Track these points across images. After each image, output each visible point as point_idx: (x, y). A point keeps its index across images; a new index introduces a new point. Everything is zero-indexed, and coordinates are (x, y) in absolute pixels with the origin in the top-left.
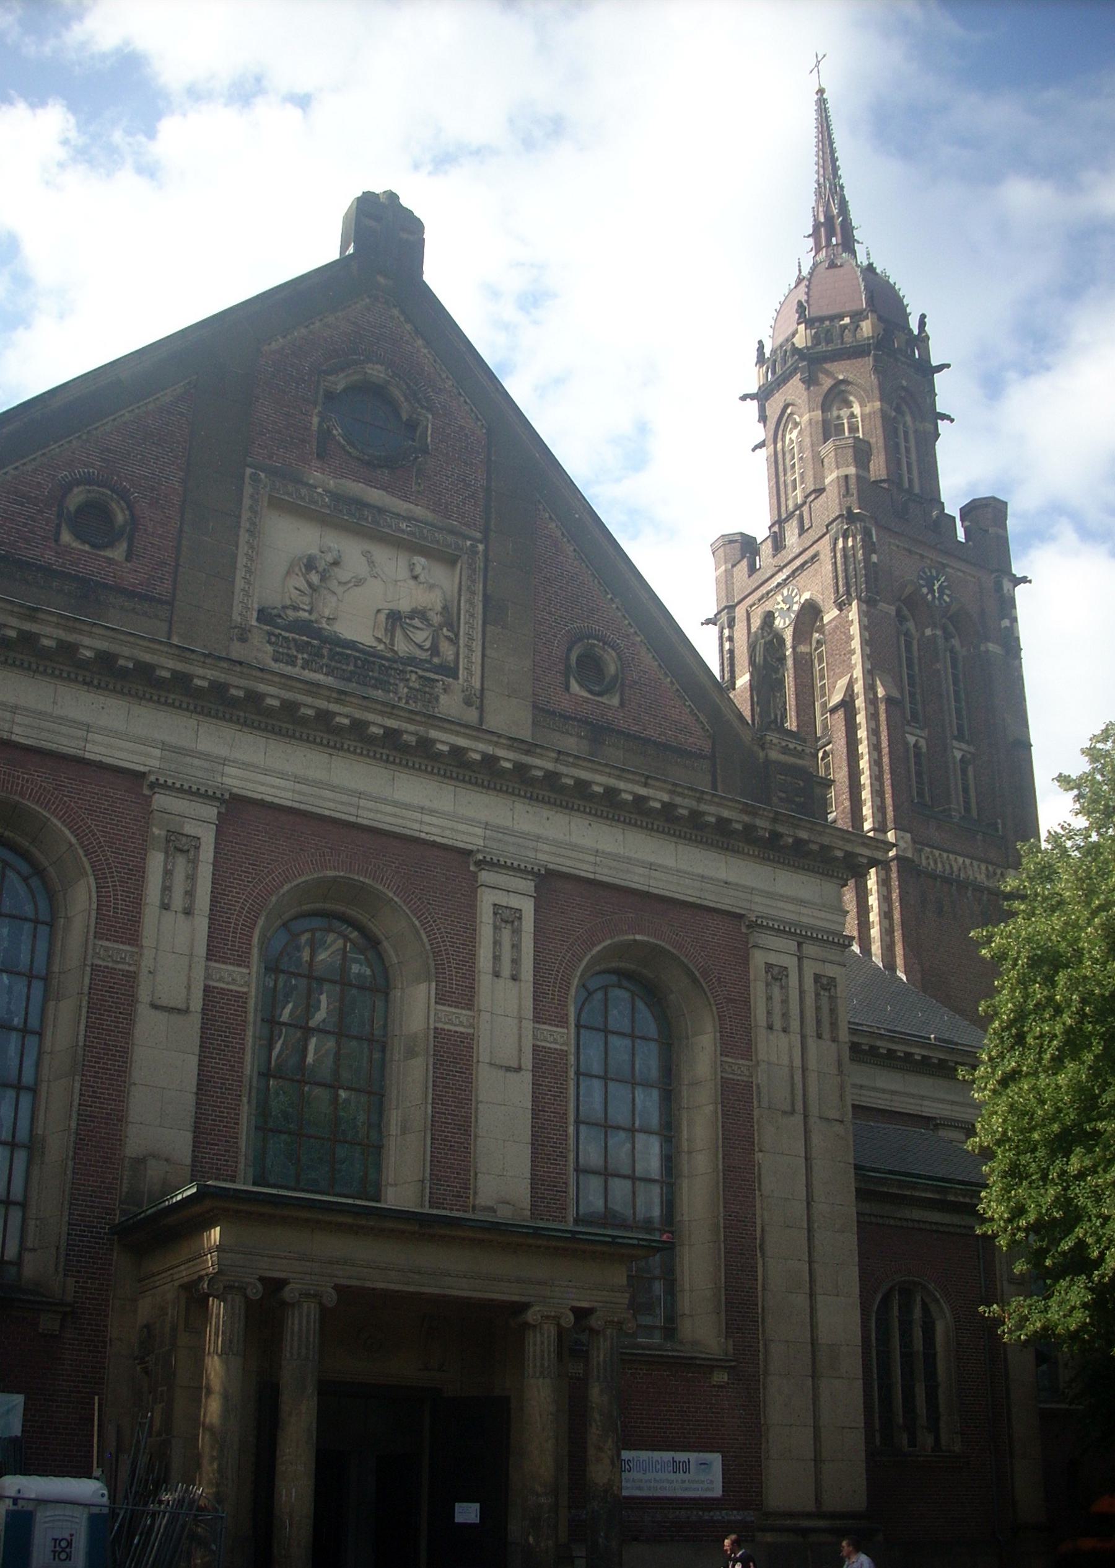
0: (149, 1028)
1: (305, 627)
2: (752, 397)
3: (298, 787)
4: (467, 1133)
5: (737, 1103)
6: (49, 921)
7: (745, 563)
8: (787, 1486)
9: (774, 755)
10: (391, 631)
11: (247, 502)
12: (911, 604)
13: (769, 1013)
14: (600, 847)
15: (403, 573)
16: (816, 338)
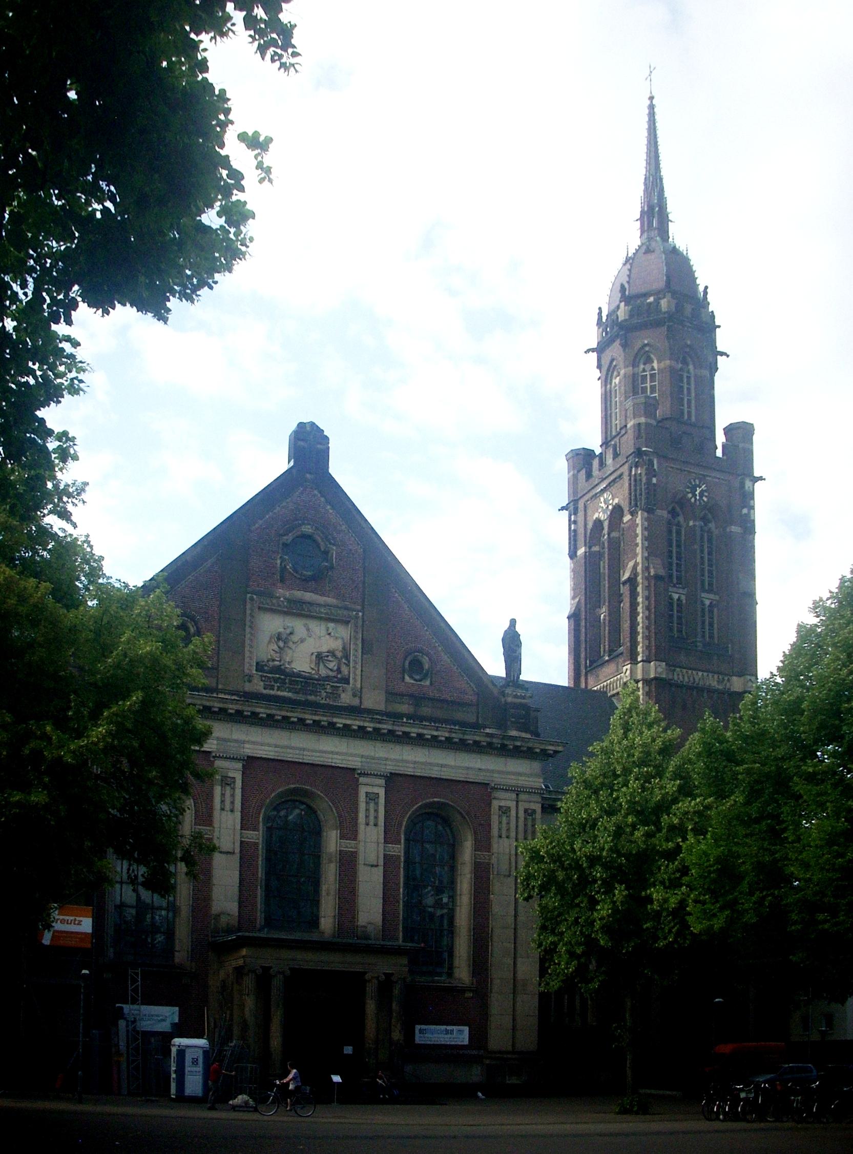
1: (278, 670)
2: (593, 350)
3: (276, 749)
4: (354, 894)
5: (482, 873)
7: (584, 471)
8: (498, 1038)
9: (510, 699)
10: (318, 664)
11: (248, 612)
12: (679, 505)
13: (500, 829)
14: (417, 759)
15: (323, 632)
16: (631, 316)
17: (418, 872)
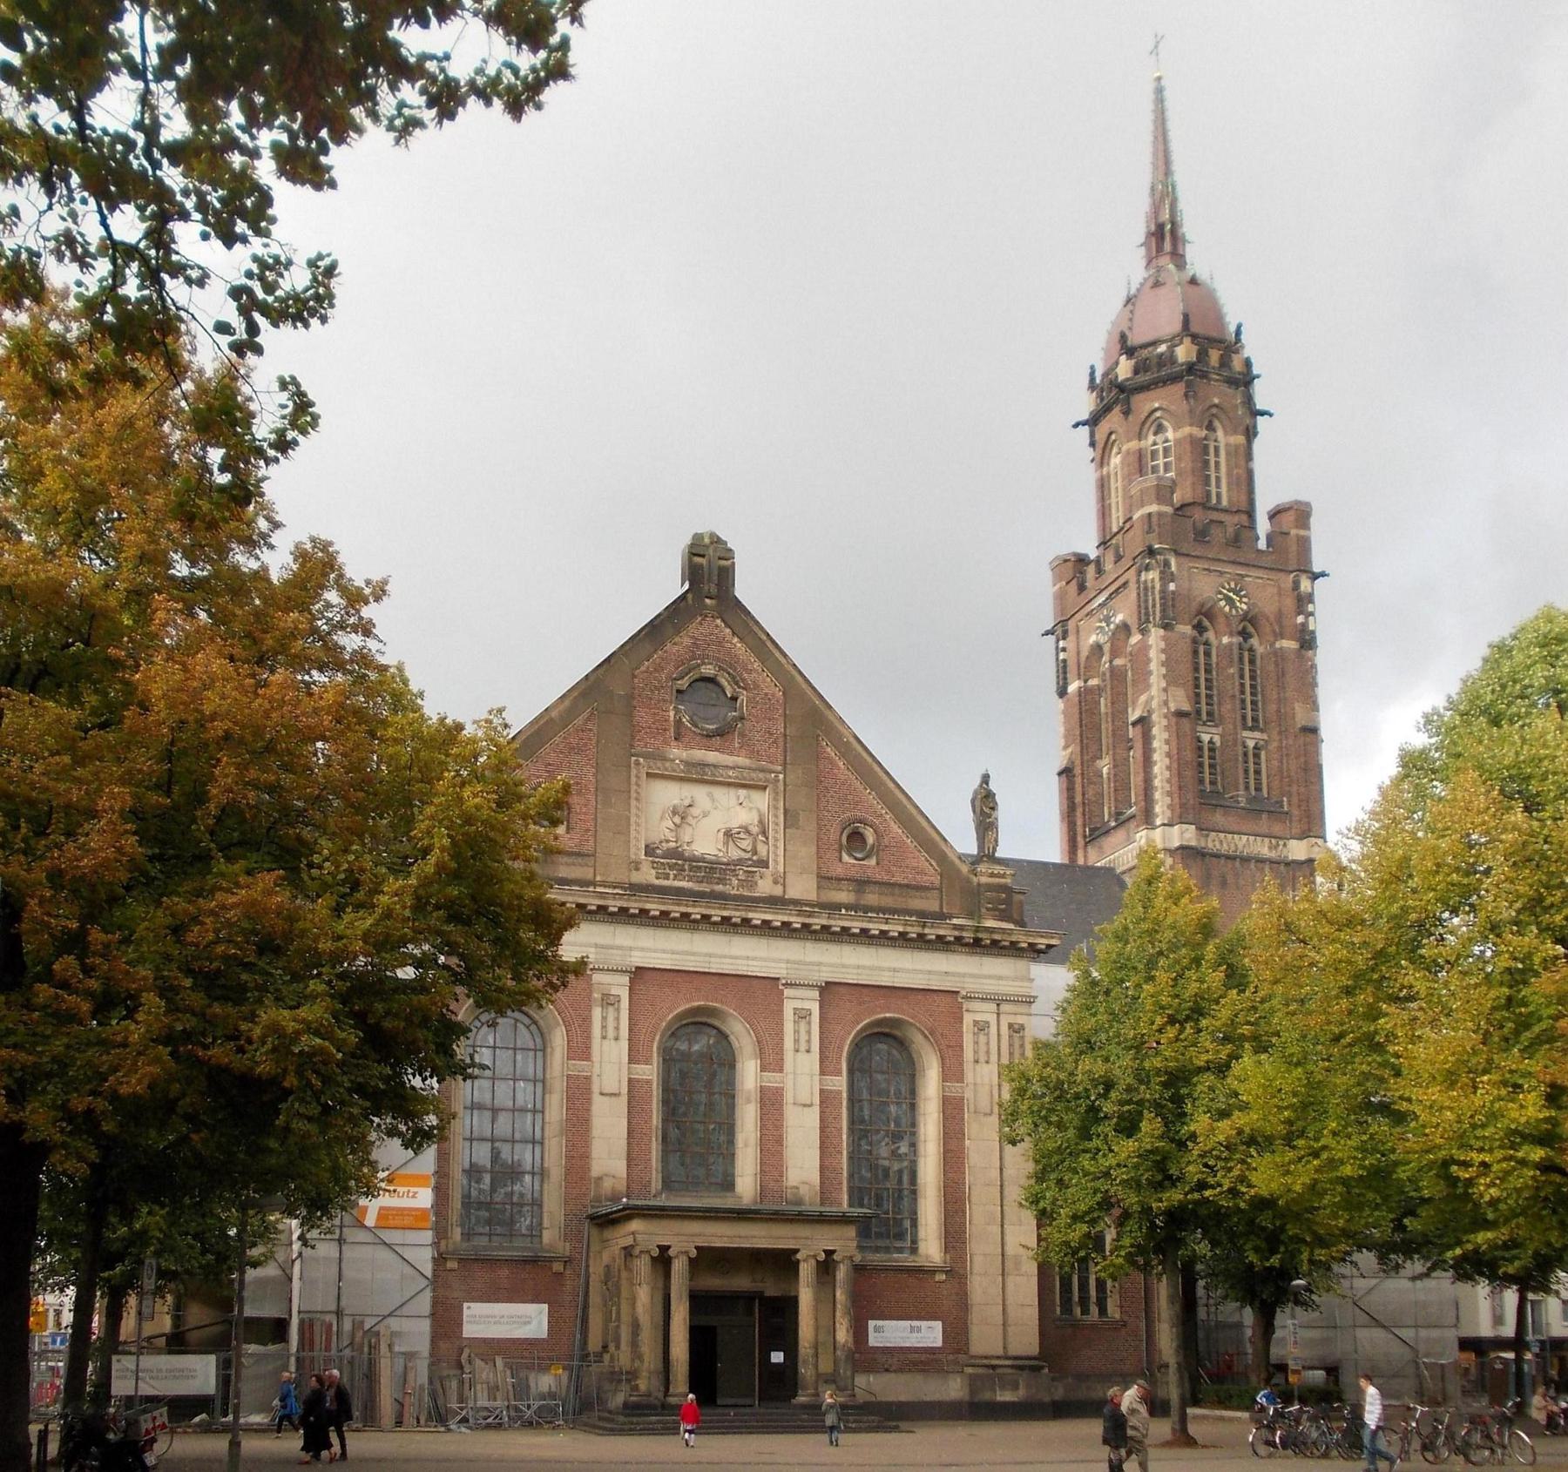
0: (599, 1105)
1: (675, 854)
6: (543, 1049)
8: (984, 1339)
9: (984, 880)
10: (726, 844)
11: (633, 779)
15: (733, 802)
16: (1136, 372)
17: (866, 1112)
